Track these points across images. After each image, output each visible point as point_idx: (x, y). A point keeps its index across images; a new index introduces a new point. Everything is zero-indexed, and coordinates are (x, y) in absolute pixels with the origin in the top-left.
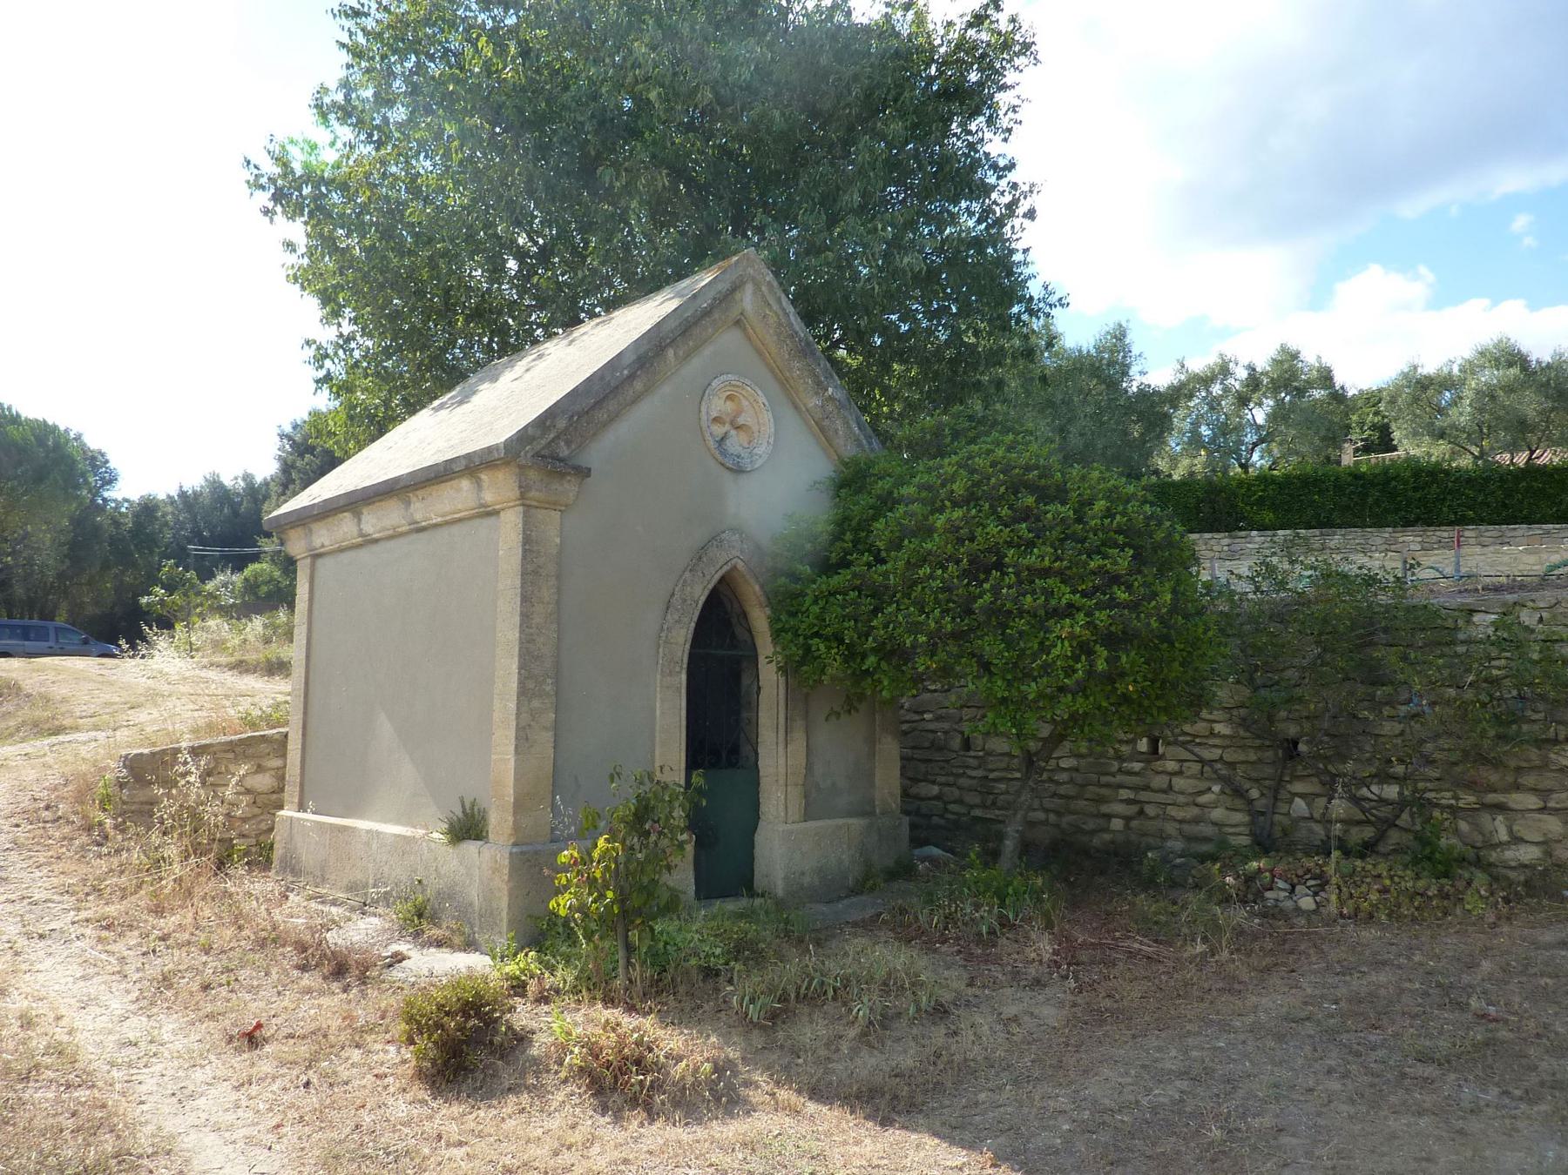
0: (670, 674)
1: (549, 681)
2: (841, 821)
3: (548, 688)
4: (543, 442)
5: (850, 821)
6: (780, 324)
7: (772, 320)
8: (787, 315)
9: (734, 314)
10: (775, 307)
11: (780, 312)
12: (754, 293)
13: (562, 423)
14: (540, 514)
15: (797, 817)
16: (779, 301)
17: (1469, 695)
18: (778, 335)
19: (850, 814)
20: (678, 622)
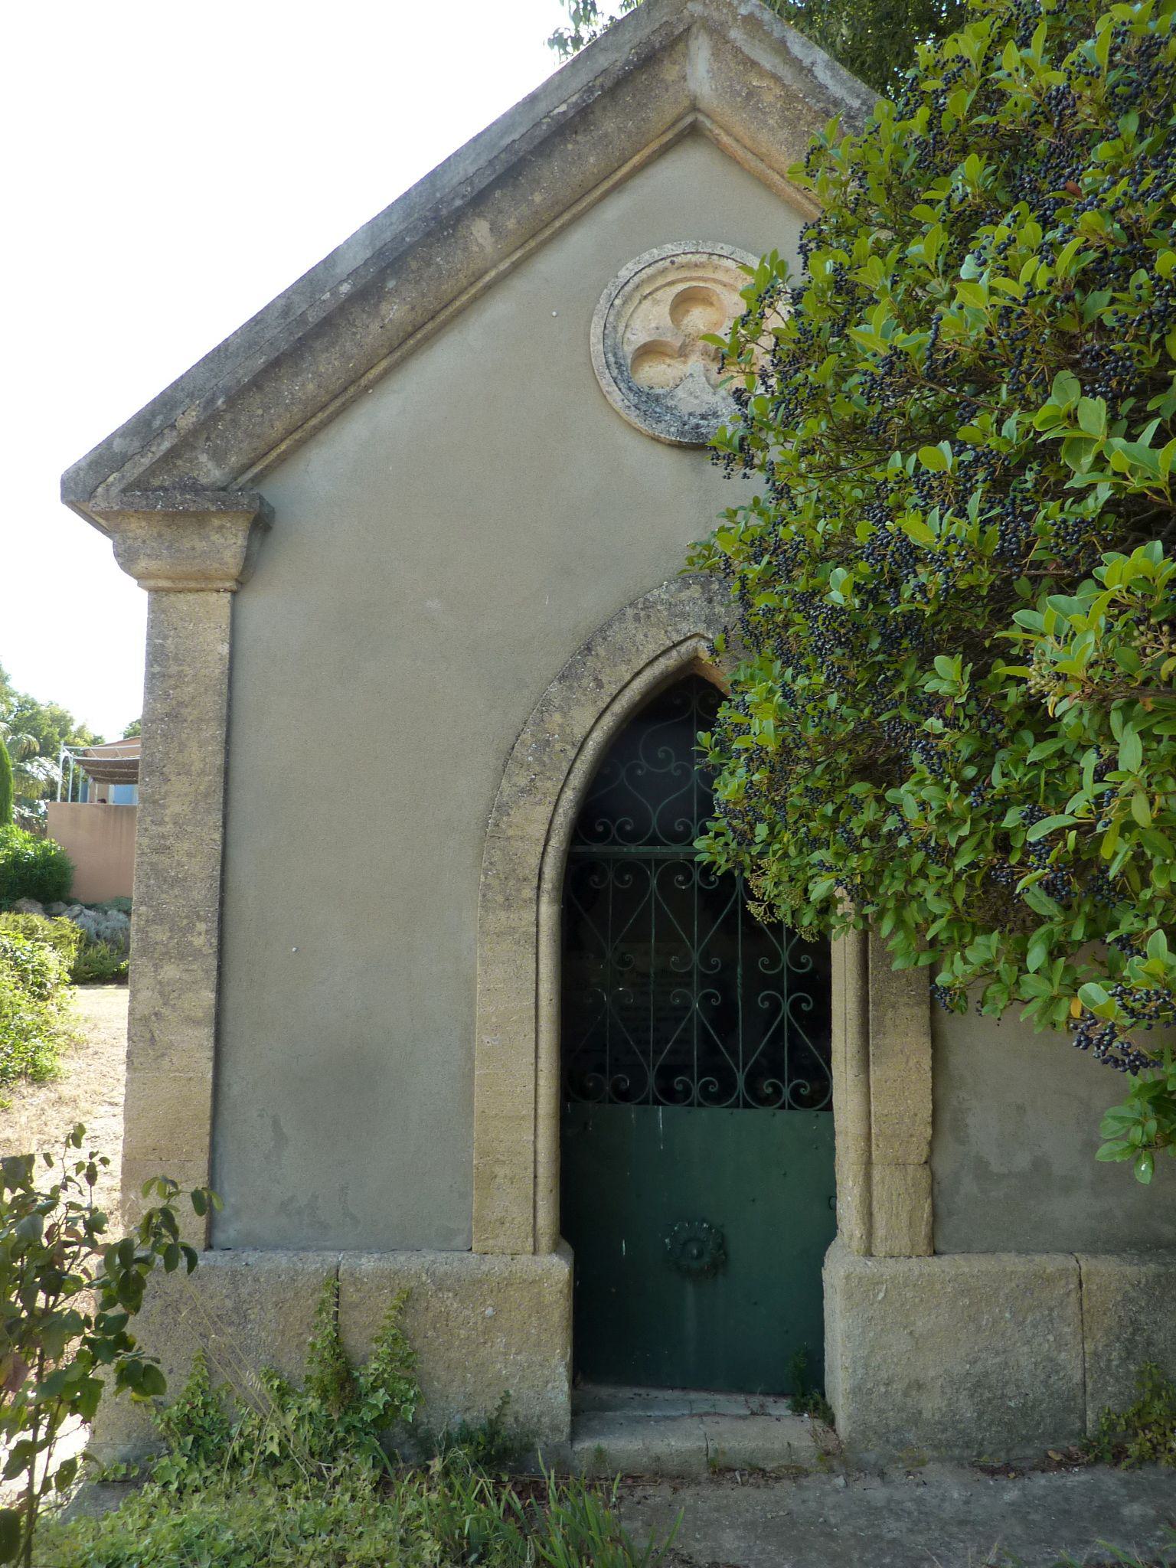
0: (508, 905)
1: (201, 927)
2: (1052, 1263)
3: (198, 941)
4: (146, 461)
5: (1087, 1264)
6: (790, 98)
7: (771, 96)
8: (805, 71)
9: (664, 111)
10: (768, 61)
11: (786, 73)
12: (716, 54)
13: (187, 420)
14: (184, 603)
15: (903, 1243)
16: (781, 48)
17: (532, 1500)
18: (792, 123)
19: (1096, 1246)
20: (528, 790)
